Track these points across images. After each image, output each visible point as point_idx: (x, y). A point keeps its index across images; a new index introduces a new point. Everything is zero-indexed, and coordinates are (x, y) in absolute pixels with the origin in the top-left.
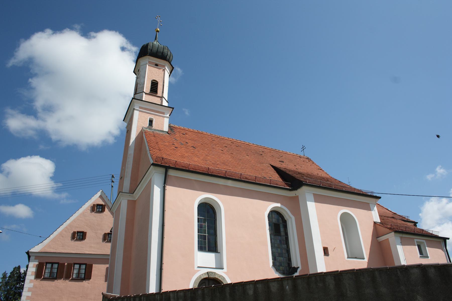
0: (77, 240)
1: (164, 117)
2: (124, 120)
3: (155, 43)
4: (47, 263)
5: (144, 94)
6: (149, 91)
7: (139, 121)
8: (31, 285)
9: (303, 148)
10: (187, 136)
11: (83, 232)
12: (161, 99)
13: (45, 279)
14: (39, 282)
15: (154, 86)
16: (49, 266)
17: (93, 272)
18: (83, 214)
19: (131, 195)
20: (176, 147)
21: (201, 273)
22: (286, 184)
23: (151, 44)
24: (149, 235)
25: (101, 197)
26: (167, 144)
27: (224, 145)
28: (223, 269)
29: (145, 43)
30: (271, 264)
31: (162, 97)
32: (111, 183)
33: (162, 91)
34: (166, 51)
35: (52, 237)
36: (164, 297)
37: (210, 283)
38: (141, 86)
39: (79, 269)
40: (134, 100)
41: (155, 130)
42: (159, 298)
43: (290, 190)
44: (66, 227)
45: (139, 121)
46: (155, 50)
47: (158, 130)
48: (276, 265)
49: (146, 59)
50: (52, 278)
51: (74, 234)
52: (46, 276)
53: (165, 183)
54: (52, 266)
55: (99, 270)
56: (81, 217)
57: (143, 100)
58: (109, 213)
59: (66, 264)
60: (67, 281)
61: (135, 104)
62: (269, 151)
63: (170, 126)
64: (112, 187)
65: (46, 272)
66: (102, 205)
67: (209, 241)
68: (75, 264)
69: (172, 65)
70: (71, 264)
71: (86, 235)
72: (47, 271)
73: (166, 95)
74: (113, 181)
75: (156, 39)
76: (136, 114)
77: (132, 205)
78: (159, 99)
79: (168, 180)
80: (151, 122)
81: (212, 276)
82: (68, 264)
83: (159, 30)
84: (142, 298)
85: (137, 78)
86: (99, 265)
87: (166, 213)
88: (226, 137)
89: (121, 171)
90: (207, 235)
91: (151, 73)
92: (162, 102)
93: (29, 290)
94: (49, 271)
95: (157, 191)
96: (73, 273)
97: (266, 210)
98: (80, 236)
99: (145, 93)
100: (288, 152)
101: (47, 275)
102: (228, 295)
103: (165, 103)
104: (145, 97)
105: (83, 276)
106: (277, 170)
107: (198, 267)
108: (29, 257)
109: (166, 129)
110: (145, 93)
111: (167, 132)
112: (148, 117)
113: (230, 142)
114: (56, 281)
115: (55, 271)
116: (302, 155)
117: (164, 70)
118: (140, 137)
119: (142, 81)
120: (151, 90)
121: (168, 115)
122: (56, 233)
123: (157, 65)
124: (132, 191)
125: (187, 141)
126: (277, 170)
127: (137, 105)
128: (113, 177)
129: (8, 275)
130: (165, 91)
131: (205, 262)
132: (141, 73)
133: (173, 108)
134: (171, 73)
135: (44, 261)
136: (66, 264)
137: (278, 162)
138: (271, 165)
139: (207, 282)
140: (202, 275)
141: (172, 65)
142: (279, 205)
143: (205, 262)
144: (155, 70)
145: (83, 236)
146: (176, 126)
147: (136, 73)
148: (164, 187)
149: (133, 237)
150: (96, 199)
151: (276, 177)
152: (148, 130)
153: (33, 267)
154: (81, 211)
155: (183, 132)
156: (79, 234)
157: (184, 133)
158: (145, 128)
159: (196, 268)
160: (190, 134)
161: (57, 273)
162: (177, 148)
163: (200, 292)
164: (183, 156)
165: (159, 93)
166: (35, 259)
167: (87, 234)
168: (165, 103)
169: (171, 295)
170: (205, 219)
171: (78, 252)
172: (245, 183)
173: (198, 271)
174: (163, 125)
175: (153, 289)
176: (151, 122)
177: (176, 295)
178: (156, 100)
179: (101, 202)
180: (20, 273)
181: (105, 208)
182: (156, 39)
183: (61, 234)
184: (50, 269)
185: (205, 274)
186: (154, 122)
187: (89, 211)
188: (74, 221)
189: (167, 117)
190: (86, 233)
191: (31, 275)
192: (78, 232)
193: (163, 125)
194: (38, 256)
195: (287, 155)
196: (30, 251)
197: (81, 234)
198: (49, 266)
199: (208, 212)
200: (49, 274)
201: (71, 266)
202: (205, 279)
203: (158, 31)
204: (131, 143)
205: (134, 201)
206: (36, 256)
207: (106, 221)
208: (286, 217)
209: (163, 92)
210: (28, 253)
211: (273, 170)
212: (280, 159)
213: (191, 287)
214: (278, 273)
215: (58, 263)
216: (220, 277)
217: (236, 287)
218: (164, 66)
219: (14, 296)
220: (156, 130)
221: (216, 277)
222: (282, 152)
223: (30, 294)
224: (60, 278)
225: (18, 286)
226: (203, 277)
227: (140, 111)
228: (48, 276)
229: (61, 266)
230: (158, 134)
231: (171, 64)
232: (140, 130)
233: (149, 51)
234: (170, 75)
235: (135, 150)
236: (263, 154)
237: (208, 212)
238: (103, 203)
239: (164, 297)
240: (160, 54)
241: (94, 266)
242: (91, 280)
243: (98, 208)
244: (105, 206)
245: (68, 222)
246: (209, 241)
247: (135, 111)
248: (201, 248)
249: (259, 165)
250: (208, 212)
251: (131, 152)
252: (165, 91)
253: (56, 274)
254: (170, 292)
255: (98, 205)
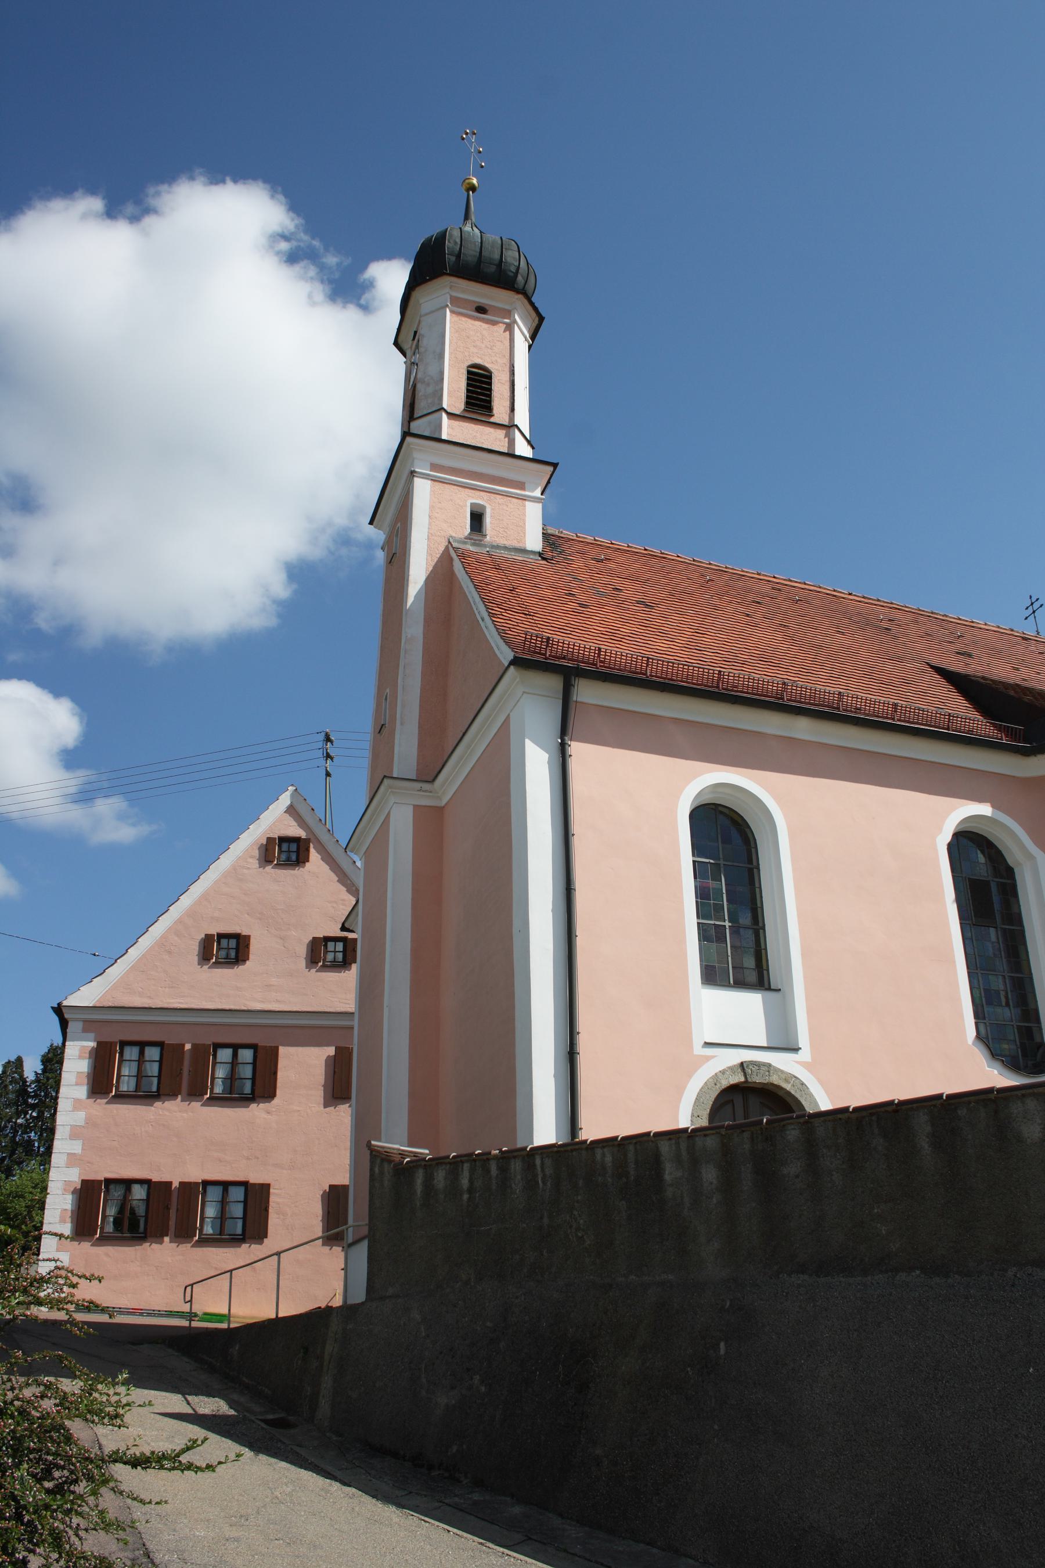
0: (218, 964)
1: (524, 499)
2: (371, 523)
3: (467, 228)
4: (124, 1044)
5: (444, 416)
6: (462, 406)
7: (436, 516)
8: (80, 1117)
9: (1033, 607)
10: (612, 565)
11: (237, 936)
12: (507, 435)
13: (121, 1097)
14: (101, 1107)
15: (479, 388)
16: (131, 1053)
17: (280, 1074)
18: (234, 872)
19: (426, 786)
20: (581, 605)
21: (719, 1067)
22: (999, 728)
23: (456, 233)
24: (515, 930)
25: (291, 810)
26: (548, 593)
27: (751, 597)
28: (796, 1050)
29: (433, 231)
30: (971, 1031)
31: (510, 427)
32: (322, 761)
33: (508, 403)
34: (511, 256)
35: (134, 953)
36: (631, 1155)
37: (753, 1105)
38: (430, 390)
39: (234, 1063)
40: (409, 439)
41: (493, 547)
42: (609, 1159)
43: (1026, 753)
44: (180, 921)
45: (436, 516)
46: (471, 253)
47: (505, 548)
48: (991, 1039)
49: (444, 289)
50: (142, 1096)
51: (207, 942)
52: (124, 1088)
53: (564, 731)
54: (142, 1053)
55: (302, 1067)
56: (227, 881)
57: (444, 437)
58: (325, 868)
59: (188, 1047)
60: (196, 1105)
61: (416, 455)
62: (910, 616)
63: (546, 536)
64: (328, 774)
65: (126, 1077)
66: (297, 840)
67: (739, 942)
68: (217, 1046)
69: (536, 309)
70: (206, 1047)
71: (248, 946)
72: (125, 1071)
73: (522, 418)
74: (328, 756)
75: (467, 217)
76: (423, 491)
77: (431, 823)
78: (500, 433)
79: (576, 722)
80: (477, 519)
81: (757, 1079)
82: (193, 1045)
83: (475, 181)
84: (538, 1162)
85: (411, 366)
86: (300, 1049)
87: (577, 843)
88: (750, 570)
89: (378, 705)
90: (727, 924)
91: (465, 339)
92: (512, 443)
93: (75, 1134)
94: (134, 1072)
95: (536, 764)
96: (213, 1078)
97: (940, 830)
98: (228, 949)
99: (449, 414)
100: (980, 622)
101: (127, 1085)
102: (924, 1144)
103: (523, 449)
104: (449, 429)
105: (248, 1089)
106: (962, 683)
107: (708, 1044)
108: (64, 1024)
109: (534, 542)
110: (449, 414)
111: (540, 554)
112: (467, 500)
113: (767, 588)
114: (158, 1104)
115: (153, 1069)
116: (1031, 633)
117: (509, 328)
118: (442, 576)
119: (432, 370)
120: (467, 403)
121: (537, 493)
122: (145, 942)
123: (481, 310)
124: (429, 773)
125: (617, 582)
126: (962, 683)
127: (422, 457)
128: (328, 739)
129: (40, 1072)
130: (517, 399)
131: (728, 1026)
132: (427, 341)
133: (555, 465)
134: (533, 337)
135: (116, 1037)
136: (188, 1047)
137: (954, 658)
138: (932, 667)
139: (738, 1100)
140: (723, 1072)
141: (536, 309)
142: (985, 809)
143: (728, 1026)
144: (476, 327)
145: (237, 949)
146: (567, 533)
147: (405, 347)
148: (563, 748)
149: (450, 933)
150: (274, 819)
151: (958, 707)
152: (471, 548)
153: (80, 1057)
154: (225, 861)
155: (594, 552)
156: (224, 942)
157: (603, 556)
158: (459, 542)
159: (698, 1050)
160: (621, 559)
161: (159, 1077)
162: (586, 606)
163: (711, 1142)
164: (613, 635)
165: (500, 412)
166: (85, 1030)
167: (252, 941)
168: (523, 449)
169: (665, 1147)
170: (717, 866)
171: (227, 1007)
172: (851, 728)
173: (708, 1058)
174: (522, 527)
175: (545, 1130)
176: (477, 519)
177: (683, 1146)
178: (493, 438)
179: (294, 830)
180: (25, 1081)
181: (308, 850)
182: (467, 217)
183: (162, 943)
184: (135, 1065)
185: (731, 1069)
186: (488, 520)
187: (255, 863)
188: (205, 897)
189: (535, 500)
190: (248, 937)
191: (77, 1084)
192: (221, 936)
193: (523, 527)
194: (95, 1019)
195: (977, 632)
196: (65, 1003)
197: (233, 943)
198: (131, 1053)
199: (727, 840)
200: (133, 1081)
201: (204, 1054)
202: (732, 1090)
203: (473, 188)
204: (410, 600)
205: (439, 812)
206: (85, 1021)
207: (319, 898)
208: (1013, 856)
209: (512, 409)
210: (58, 1010)
211: (943, 682)
212: (958, 646)
213: (684, 1121)
214: (998, 1064)
215: (160, 1044)
216: (786, 1081)
217: (962, 1112)
218: (508, 313)
219: (13, 1153)
220: (498, 547)
221: (775, 1079)
222: (960, 623)
223: (76, 1147)
224: (173, 1094)
225: (19, 1121)
226: (725, 1083)
227: (435, 480)
228: (132, 1087)
229: (170, 1053)
230: (507, 560)
231: (532, 304)
232: (442, 549)
233: (450, 259)
234: (530, 347)
235: (428, 621)
236: (895, 630)
237: (727, 841)
238: (302, 834)
239: (631, 1155)
240: (493, 269)
241: (282, 1050)
242: (276, 1101)
243: (286, 852)
244: (307, 841)
245: (186, 901)
246: (739, 942)
247: (418, 482)
248: (712, 976)
249: (889, 666)
250: (727, 841)
251: (414, 630)
252: (517, 399)
253: (155, 1081)
254: (659, 1135)
255: (283, 840)
